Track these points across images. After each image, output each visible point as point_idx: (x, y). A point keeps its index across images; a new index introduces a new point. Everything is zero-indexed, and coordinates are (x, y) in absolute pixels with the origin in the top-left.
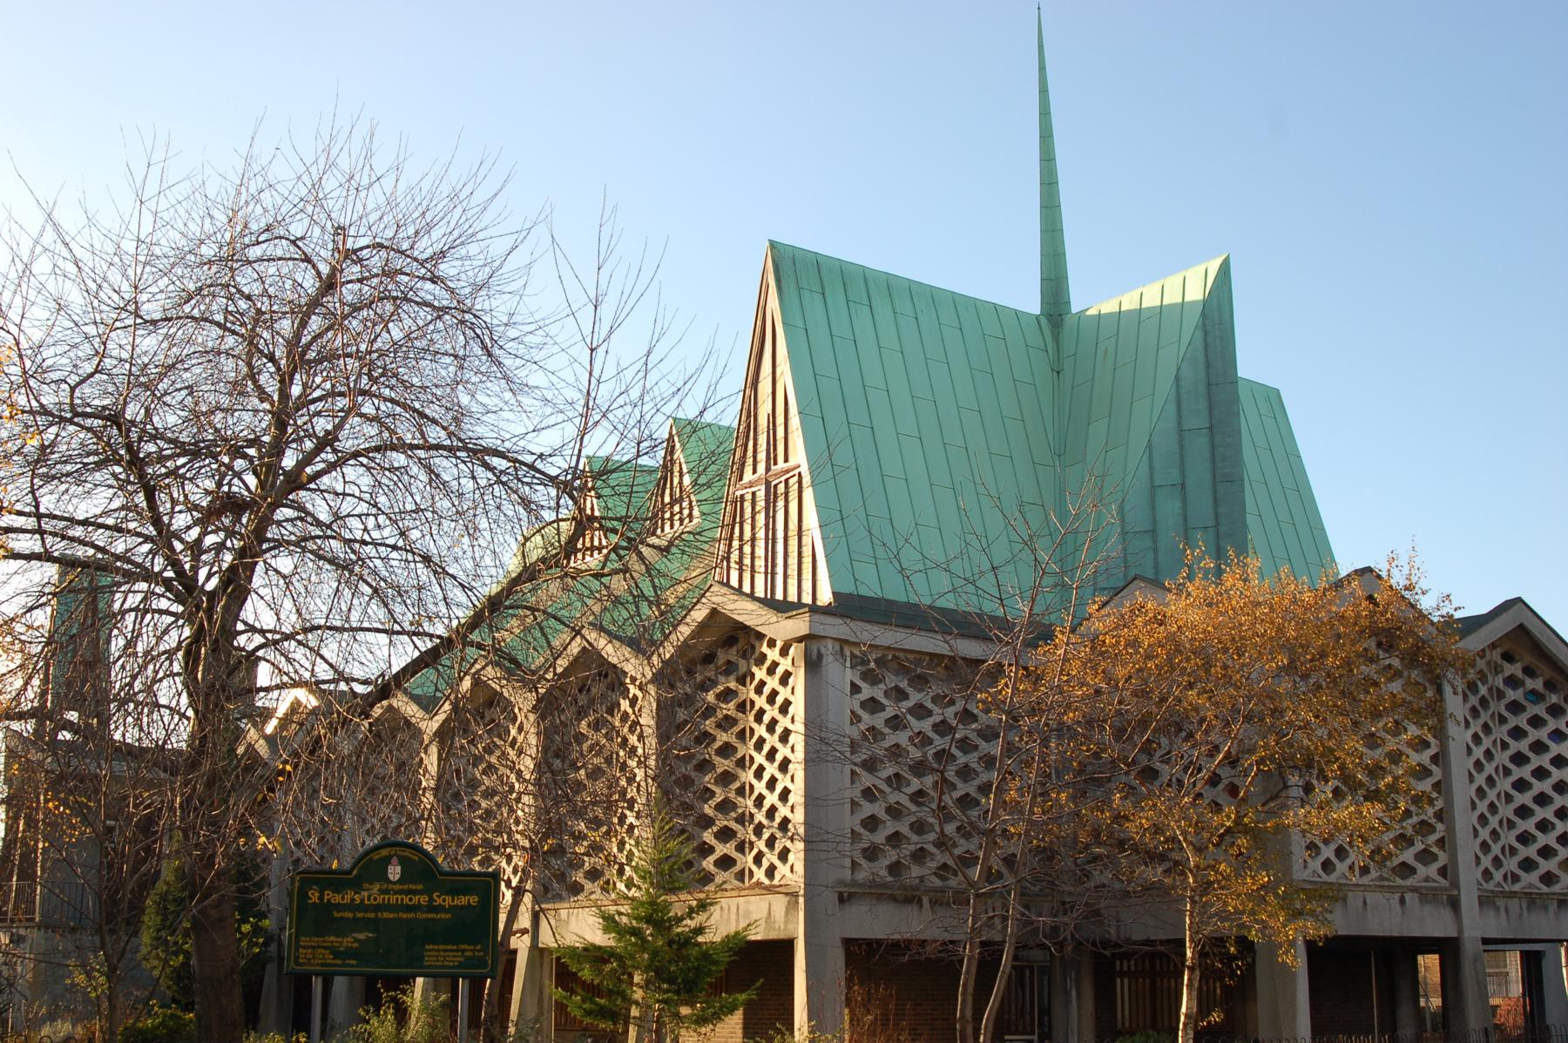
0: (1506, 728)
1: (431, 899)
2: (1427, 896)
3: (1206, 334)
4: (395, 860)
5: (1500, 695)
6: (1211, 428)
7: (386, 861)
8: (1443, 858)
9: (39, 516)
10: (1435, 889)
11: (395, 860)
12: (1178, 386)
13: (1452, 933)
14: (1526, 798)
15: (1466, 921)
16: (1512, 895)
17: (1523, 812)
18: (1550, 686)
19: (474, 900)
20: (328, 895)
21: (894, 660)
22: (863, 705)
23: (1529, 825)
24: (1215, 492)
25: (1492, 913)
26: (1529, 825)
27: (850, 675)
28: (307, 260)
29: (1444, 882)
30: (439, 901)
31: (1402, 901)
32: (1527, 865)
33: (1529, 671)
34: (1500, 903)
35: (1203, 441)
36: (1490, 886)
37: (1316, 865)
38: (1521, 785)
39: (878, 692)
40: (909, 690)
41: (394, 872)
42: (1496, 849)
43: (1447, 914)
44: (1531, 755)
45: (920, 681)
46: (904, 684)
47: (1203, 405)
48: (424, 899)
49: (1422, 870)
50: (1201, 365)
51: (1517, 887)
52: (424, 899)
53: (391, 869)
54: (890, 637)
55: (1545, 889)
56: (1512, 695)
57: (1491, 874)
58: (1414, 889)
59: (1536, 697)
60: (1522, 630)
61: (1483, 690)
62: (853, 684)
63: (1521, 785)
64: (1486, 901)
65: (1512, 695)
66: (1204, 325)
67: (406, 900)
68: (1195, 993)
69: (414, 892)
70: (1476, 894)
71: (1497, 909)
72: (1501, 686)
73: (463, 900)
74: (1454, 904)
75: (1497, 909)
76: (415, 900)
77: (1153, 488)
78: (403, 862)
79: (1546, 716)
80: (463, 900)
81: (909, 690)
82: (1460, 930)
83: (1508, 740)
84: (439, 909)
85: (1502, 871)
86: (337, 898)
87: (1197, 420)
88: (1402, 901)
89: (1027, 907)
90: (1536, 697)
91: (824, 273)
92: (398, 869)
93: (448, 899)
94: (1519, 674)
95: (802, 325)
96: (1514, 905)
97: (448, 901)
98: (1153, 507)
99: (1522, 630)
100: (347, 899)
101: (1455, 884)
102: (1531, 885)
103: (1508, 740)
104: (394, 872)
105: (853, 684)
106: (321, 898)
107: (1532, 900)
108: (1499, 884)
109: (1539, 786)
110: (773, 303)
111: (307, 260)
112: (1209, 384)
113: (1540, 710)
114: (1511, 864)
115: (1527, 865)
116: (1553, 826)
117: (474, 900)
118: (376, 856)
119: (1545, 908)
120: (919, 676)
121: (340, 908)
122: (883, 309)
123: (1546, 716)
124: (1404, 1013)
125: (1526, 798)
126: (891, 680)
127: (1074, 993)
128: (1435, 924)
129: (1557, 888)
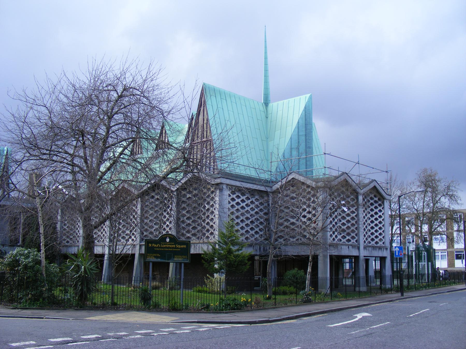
0: (370, 209)
1: (176, 246)
2: (353, 246)
3: (305, 112)
4: (168, 237)
5: (369, 201)
6: (306, 135)
7: (166, 238)
8: (357, 238)
9: (50, 151)
10: (355, 245)
11: (168, 237)
12: (298, 124)
13: (358, 255)
14: (373, 225)
15: (361, 252)
16: (370, 246)
17: (372, 228)
18: (379, 199)
19: (185, 246)
20: (153, 245)
21: (239, 189)
22: (231, 199)
23: (373, 231)
24: (306, 150)
25: (366, 250)
26: (373, 231)
27: (229, 192)
28: (116, 90)
29: (356, 243)
30: (178, 246)
31: (348, 248)
32: (373, 240)
33: (375, 196)
34: (367, 248)
35: (303, 138)
36: (365, 244)
37: (332, 239)
38: (372, 222)
39: (234, 196)
40: (241, 196)
41: (168, 240)
42: (366, 236)
43: (357, 251)
44: (374, 215)
45: (243, 194)
46: (240, 195)
47: (304, 129)
48: (174, 246)
49: (352, 241)
50: (304, 120)
51: (370, 245)
52: (174, 246)
53: (167, 239)
54: (238, 184)
55: (376, 245)
56: (371, 201)
57: (332, 229)
58: (351, 245)
59: (376, 202)
60: (375, 187)
61: (366, 200)
62: (229, 194)
63: (372, 222)
64: (365, 248)
65: (371, 201)
66: (305, 110)
67: (170, 246)
68: (311, 267)
69: (172, 245)
70: (363, 246)
71: (367, 250)
72: (369, 199)
73: (183, 246)
74: (359, 248)
75: (367, 250)
76: (172, 246)
77: (291, 149)
78: (170, 238)
79: (378, 206)
80: (183, 246)
81: (241, 196)
82: (360, 254)
83: (370, 211)
84: (178, 248)
85: (367, 241)
86: (155, 246)
87: (302, 133)
88: (348, 248)
89: (93, 229)
90: (376, 202)
91: (216, 91)
92: (169, 239)
93: (180, 246)
94: (373, 197)
95: (211, 104)
96: (370, 249)
97: (179, 246)
98: (291, 152)
99: (375, 187)
100: (157, 246)
101: (359, 244)
102: (373, 244)
103: (370, 211)
104: (168, 240)
105: (229, 194)
106: (152, 245)
107: (374, 248)
108: (367, 244)
109: (244, 225)
110: (434, 264)
111: (116, 90)
112: (306, 125)
113: (377, 205)
114: (369, 239)
115: (373, 240)
116: (378, 231)
117: (185, 246)
118: (164, 237)
119: (376, 250)
120: (243, 193)
121: (156, 247)
122: (228, 100)
123: (378, 206)
124: (340, 272)
125: (373, 225)
126: (237, 194)
127: (273, 267)
128: (354, 253)
129: (378, 245)
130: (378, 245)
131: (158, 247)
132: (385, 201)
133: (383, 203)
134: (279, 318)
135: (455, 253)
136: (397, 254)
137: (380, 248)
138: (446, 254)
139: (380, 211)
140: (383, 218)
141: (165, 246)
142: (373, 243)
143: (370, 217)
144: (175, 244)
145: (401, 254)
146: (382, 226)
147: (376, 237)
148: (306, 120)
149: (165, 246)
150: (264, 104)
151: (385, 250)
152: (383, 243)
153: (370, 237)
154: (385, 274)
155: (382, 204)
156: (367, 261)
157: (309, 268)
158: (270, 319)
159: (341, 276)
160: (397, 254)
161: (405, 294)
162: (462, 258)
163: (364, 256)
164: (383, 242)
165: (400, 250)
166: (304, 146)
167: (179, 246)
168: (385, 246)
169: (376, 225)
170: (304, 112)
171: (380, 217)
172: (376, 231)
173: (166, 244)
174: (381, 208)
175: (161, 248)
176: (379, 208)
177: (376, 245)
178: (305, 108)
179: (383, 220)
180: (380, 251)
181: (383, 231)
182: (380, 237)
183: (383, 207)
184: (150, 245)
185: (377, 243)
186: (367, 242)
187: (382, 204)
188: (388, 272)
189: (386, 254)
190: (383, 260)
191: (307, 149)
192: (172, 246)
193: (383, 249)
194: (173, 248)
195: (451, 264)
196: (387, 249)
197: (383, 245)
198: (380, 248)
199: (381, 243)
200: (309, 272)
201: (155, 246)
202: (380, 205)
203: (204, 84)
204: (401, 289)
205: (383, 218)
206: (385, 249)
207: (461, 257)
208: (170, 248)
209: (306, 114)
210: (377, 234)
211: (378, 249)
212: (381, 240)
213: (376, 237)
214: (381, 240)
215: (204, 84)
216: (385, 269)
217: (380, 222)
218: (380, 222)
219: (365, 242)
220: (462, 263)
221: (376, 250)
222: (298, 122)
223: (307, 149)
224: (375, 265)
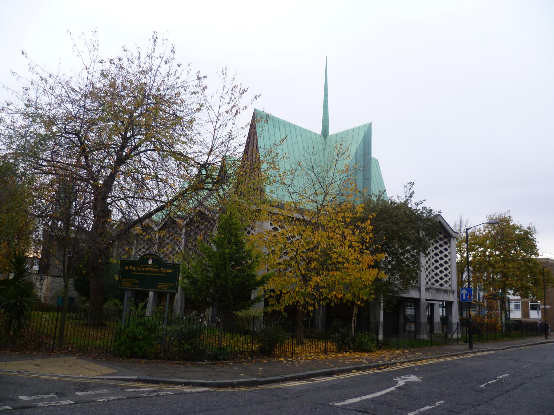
3: (364, 142)
4: (151, 258)
7: (148, 259)
11: (151, 258)
13: (418, 297)
14: (437, 265)
15: (422, 294)
16: (433, 289)
18: (445, 237)
19: (172, 271)
30: (163, 271)
32: (437, 281)
34: (430, 290)
36: (428, 286)
41: (150, 262)
43: (417, 292)
44: (439, 254)
47: (362, 160)
48: (158, 270)
51: (434, 287)
52: (158, 270)
53: (149, 261)
55: (440, 287)
64: (427, 289)
67: (153, 270)
68: (357, 308)
71: (429, 292)
73: (169, 271)
74: (419, 290)
75: (429, 292)
76: (156, 270)
78: (153, 259)
79: (443, 244)
80: (169, 271)
82: (421, 296)
84: (163, 273)
86: (134, 268)
92: (152, 261)
96: (433, 291)
97: (165, 271)
102: (437, 286)
104: (150, 262)
106: (129, 268)
107: (438, 290)
114: (433, 281)
115: (437, 281)
117: (172, 271)
121: (134, 271)
123: (443, 244)
125: (437, 265)
129: (443, 288)
130: (443, 288)
131: (137, 271)
132: (452, 240)
133: (450, 241)
134: (279, 378)
135: (530, 304)
136: (464, 298)
137: (446, 291)
138: (520, 304)
139: (446, 249)
140: (449, 257)
141: (146, 269)
142: (437, 285)
143: (434, 256)
144: (159, 268)
145: (470, 298)
146: (448, 267)
147: (441, 278)
148: (364, 150)
149: (146, 269)
150: (322, 136)
151: (451, 294)
152: (450, 286)
153: (433, 278)
154: (452, 320)
155: (448, 242)
156: (431, 307)
157: (355, 309)
158: (261, 380)
159: (401, 321)
160: (464, 298)
161: (474, 346)
162: (538, 309)
163: (427, 300)
164: (449, 284)
165: (468, 293)
166: (362, 178)
167: (165, 271)
168: (452, 290)
169: (441, 265)
170: (363, 142)
171: (446, 256)
172: (441, 272)
173: (148, 267)
174: (447, 247)
175: (141, 271)
176: (445, 246)
177: (440, 287)
178: (364, 137)
179: (449, 260)
180: (445, 295)
181: (449, 266)
182: (446, 279)
183: (449, 245)
184: (127, 268)
185: (441, 285)
186: (430, 283)
187: (448, 242)
188: (455, 318)
189: (453, 298)
190: (449, 304)
191: (366, 181)
192: (156, 270)
193: (448, 293)
194: (156, 272)
195: (526, 314)
196: (453, 293)
197: (450, 288)
198: (446, 291)
199: (446, 286)
200: (355, 314)
201: (134, 268)
202: (446, 243)
203: (255, 110)
204: (470, 341)
205: (449, 257)
206: (451, 293)
207: (537, 307)
208: (153, 272)
209: (365, 143)
210: (442, 275)
211: (442, 292)
212: (446, 282)
213: (441, 278)
214: (446, 282)
215: (255, 110)
216: (451, 315)
217: (446, 262)
218: (446, 262)
219: (427, 283)
220: (538, 314)
221: (441, 293)
222: (356, 153)
223: (366, 181)
224: (439, 312)
